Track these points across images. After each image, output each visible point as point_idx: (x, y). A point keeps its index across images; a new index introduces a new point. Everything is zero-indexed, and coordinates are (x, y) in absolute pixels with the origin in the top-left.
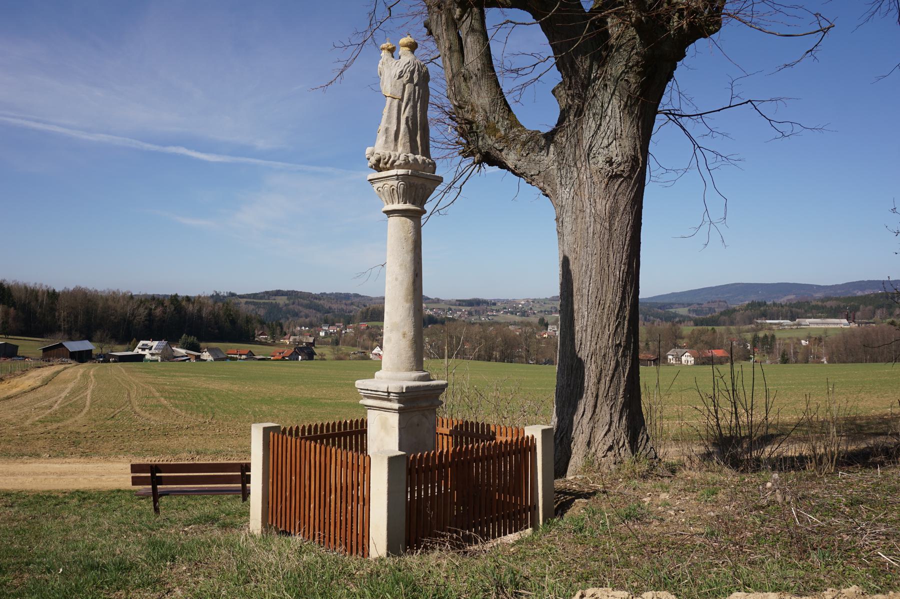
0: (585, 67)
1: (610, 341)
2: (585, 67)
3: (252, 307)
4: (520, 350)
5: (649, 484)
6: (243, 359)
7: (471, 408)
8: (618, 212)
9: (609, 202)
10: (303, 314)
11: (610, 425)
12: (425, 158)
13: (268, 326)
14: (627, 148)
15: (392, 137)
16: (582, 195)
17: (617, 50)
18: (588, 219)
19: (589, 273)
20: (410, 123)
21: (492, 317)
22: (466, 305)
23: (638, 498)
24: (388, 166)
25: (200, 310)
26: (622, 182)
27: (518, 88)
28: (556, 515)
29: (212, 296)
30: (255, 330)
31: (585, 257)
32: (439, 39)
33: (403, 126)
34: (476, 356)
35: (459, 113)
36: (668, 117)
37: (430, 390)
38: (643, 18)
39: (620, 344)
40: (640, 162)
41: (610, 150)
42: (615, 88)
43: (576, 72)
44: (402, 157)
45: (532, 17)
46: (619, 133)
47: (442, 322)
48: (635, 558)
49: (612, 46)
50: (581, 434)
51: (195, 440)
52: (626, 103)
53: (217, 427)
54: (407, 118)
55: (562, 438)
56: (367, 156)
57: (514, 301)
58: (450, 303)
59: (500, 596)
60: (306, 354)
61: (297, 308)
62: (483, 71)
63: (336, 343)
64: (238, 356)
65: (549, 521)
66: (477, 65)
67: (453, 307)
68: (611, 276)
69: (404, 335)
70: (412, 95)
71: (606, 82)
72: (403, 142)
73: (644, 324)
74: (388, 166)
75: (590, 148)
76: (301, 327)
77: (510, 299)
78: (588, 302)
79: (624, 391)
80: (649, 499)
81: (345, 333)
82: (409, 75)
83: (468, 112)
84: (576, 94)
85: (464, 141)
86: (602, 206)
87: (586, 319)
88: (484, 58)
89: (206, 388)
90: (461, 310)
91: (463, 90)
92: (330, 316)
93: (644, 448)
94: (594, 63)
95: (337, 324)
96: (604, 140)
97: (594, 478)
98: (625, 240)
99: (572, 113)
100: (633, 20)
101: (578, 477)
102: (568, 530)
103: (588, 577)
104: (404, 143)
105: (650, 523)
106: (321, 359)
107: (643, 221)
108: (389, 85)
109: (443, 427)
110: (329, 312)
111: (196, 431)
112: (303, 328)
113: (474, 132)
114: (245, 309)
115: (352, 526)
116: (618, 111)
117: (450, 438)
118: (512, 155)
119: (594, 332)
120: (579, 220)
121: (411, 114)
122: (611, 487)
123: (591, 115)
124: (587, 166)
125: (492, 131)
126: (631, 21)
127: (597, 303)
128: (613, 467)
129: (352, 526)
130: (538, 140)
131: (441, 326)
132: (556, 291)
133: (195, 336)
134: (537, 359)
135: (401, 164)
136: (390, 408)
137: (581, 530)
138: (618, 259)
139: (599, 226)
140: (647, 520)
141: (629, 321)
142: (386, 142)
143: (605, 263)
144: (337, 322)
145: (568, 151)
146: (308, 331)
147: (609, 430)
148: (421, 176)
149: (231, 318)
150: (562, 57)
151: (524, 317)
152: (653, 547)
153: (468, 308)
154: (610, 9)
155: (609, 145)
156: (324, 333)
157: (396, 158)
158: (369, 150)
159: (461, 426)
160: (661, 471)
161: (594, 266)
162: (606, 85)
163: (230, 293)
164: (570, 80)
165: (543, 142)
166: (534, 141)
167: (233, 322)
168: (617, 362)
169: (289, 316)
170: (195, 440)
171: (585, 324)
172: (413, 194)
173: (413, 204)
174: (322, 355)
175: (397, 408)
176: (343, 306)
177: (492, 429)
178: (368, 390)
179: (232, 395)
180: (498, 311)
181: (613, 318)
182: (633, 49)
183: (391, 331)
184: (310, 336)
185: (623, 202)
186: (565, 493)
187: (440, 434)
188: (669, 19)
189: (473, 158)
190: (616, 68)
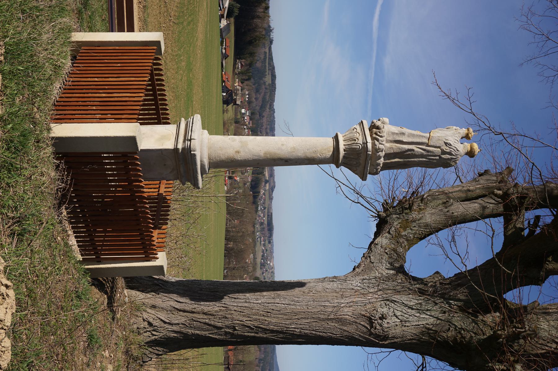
0: (459, 296)
1: (238, 322)
2: (459, 296)
3: (262, 57)
4: (234, 263)
5: (120, 355)
6: (222, 51)
7: (183, 216)
8: (342, 325)
9: (350, 317)
10: (258, 96)
11: (169, 324)
12: (381, 165)
13: (248, 70)
14: (394, 331)
15: (398, 138)
16: (355, 296)
17: (473, 321)
18: (336, 301)
19: (293, 303)
20: (409, 152)
21: (259, 241)
22: (268, 220)
23: (108, 347)
24: (374, 135)
25: (259, 17)
26: (367, 328)
27: (440, 242)
28: (93, 279)
29: (269, 27)
30: (245, 59)
31: (304, 300)
32: (476, 182)
33: (406, 147)
34: (229, 229)
35: (418, 198)
36: (421, 366)
37: (194, 174)
38: (501, 340)
39: (235, 330)
40: (384, 342)
41: (392, 318)
42: (443, 320)
43: (455, 287)
44: (381, 147)
45: (498, 252)
46: (406, 325)
47: (255, 203)
48: (52, 340)
49: (477, 317)
50: (161, 300)
51: (156, 7)
52: (431, 330)
53: (167, 25)
54: (413, 150)
55: (158, 285)
56: (381, 119)
57: (272, 257)
58: (270, 208)
59: (11, 221)
60: (228, 98)
61: (263, 91)
62: (451, 217)
63: (237, 122)
64: (224, 46)
65: (88, 273)
66: (456, 212)
67: (266, 210)
68: (290, 321)
69: (238, 152)
70: (431, 154)
71: (447, 313)
72: (394, 147)
73: (256, 359)
74: (374, 135)
75: (393, 301)
76: (248, 95)
77: (274, 254)
78: (269, 303)
79: (198, 335)
80: (108, 356)
81: (245, 128)
82: (448, 151)
83: (419, 206)
84: (437, 289)
85: (395, 205)
86: (347, 312)
87: (255, 302)
88: (462, 218)
89: (198, 21)
90: (264, 216)
91: (436, 201)
92: (257, 116)
93: (151, 352)
94: (462, 303)
95: (251, 122)
96: (400, 313)
97: (124, 311)
98: (320, 332)
99: (421, 286)
100: (499, 332)
101: (127, 298)
102: (78, 286)
103: (32, 297)
104: (393, 148)
105: (85, 355)
106: (223, 110)
107: (336, 346)
108: (439, 135)
109: (165, 188)
110: (260, 116)
111: (163, 9)
112: (247, 96)
113: (403, 211)
114: (261, 51)
115: (81, 110)
116: (424, 323)
117: (156, 194)
118: (385, 241)
119: (245, 308)
120: (335, 294)
121: (417, 153)
122: (118, 325)
123: (420, 301)
124: (379, 300)
125: (404, 225)
126: (498, 330)
127: (269, 311)
128: (135, 326)
129: (81, 110)
130: (398, 261)
131: (252, 202)
132: (278, 278)
133: (239, 14)
134: (228, 276)
135: (376, 145)
136: (178, 142)
137: (78, 297)
138: (304, 326)
139: (330, 310)
140: (88, 353)
141: (254, 337)
142: (393, 133)
143: (301, 316)
144: (252, 122)
145: (390, 284)
146: (245, 100)
147: (165, 322)
148: (367, 162)
149: (253, 41)
150: (466, 276)
151: (260, 265)
152: (62, 355)
153: (266, 222)
154: (508, 315)
155: (396, 316)
156: (244, 112)
157: (380, 141)
158: (386, 120)
159: (166, 203)
160: (132, 367)
161: (298, 307)
162: (445, 312)
163: (273, 40)
164: (448, 284)
165: (397, 265)
166: (398, 258)
167: (250, 43)
168: (219, 328)
169: (256, 85)
170: (156, 7)
171: (251, 301)
172: (352, 157)
173: (344, 157)
174: (227, 110)
175: (178, 147)
176: (264, 127)
177: (164, 227)
178: (193, 123)
179: (193, 40)
180: (264, 245)
181: (256, 324)
182: (475, 333)
183: (241, 142)
184: (241, 102)
185: (351, 329)
186: (112, 288)
187: (160, 186)
188: (501, 362)
189: (382, 211)
190: (459, 320)
